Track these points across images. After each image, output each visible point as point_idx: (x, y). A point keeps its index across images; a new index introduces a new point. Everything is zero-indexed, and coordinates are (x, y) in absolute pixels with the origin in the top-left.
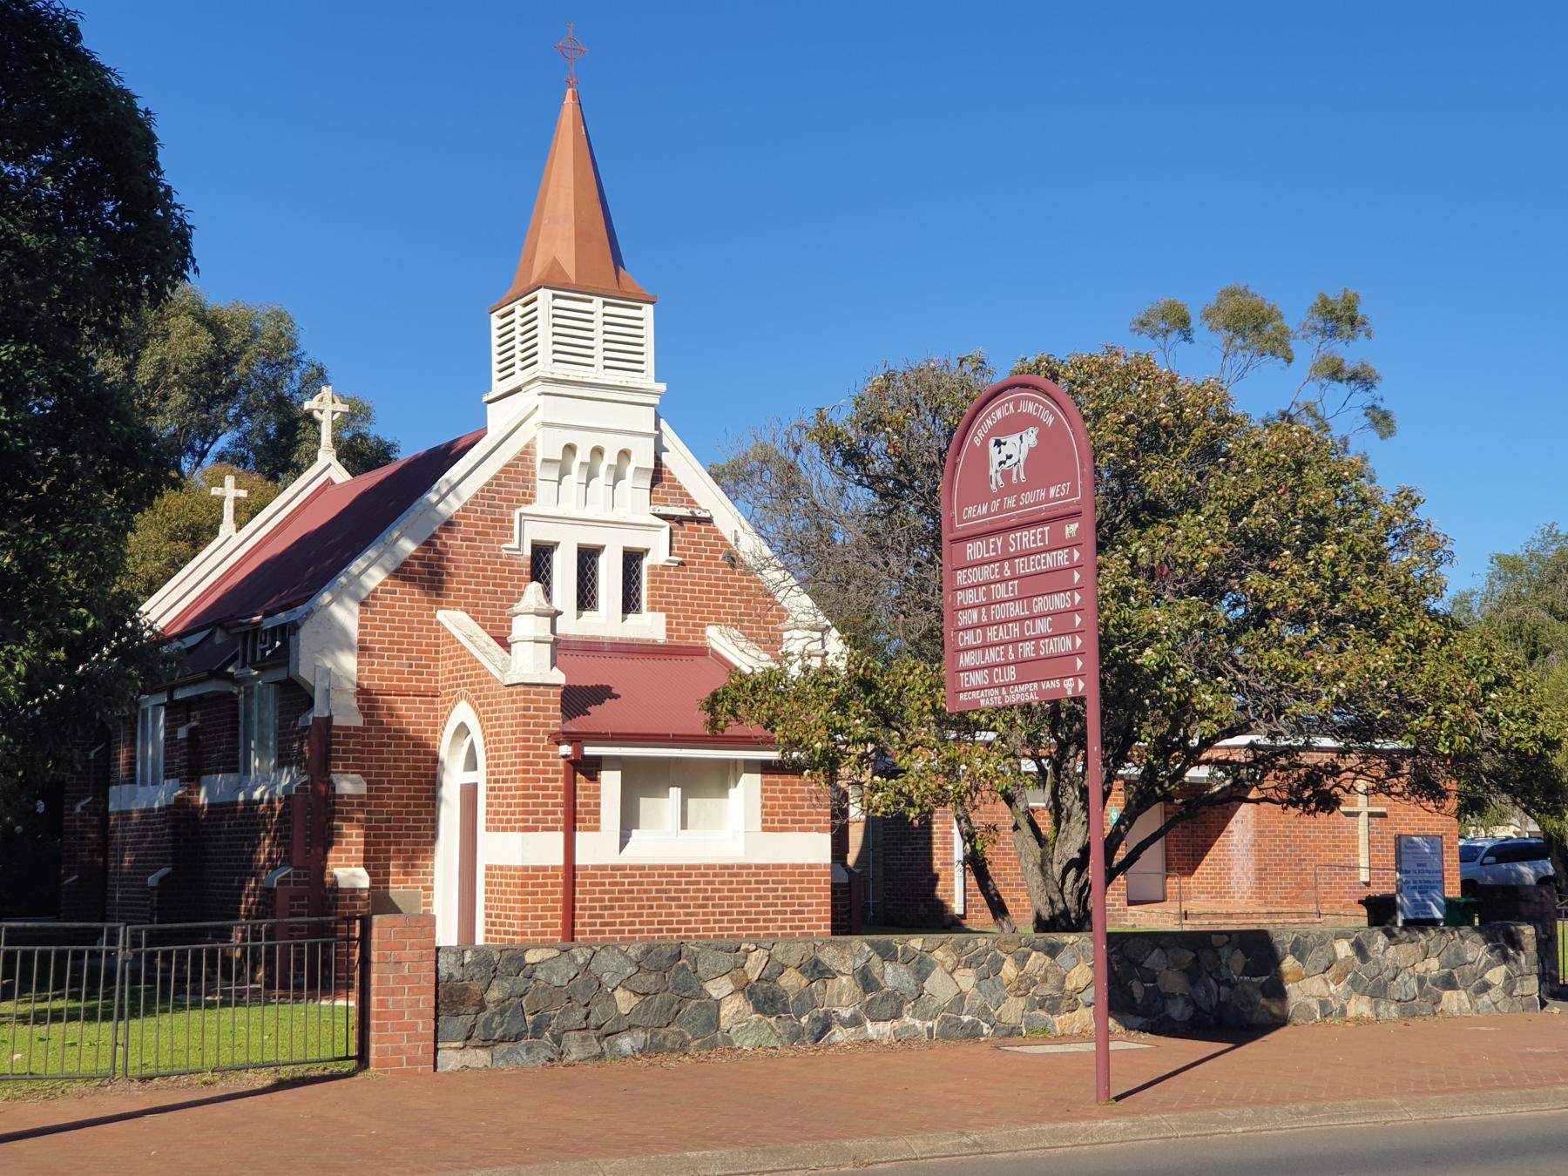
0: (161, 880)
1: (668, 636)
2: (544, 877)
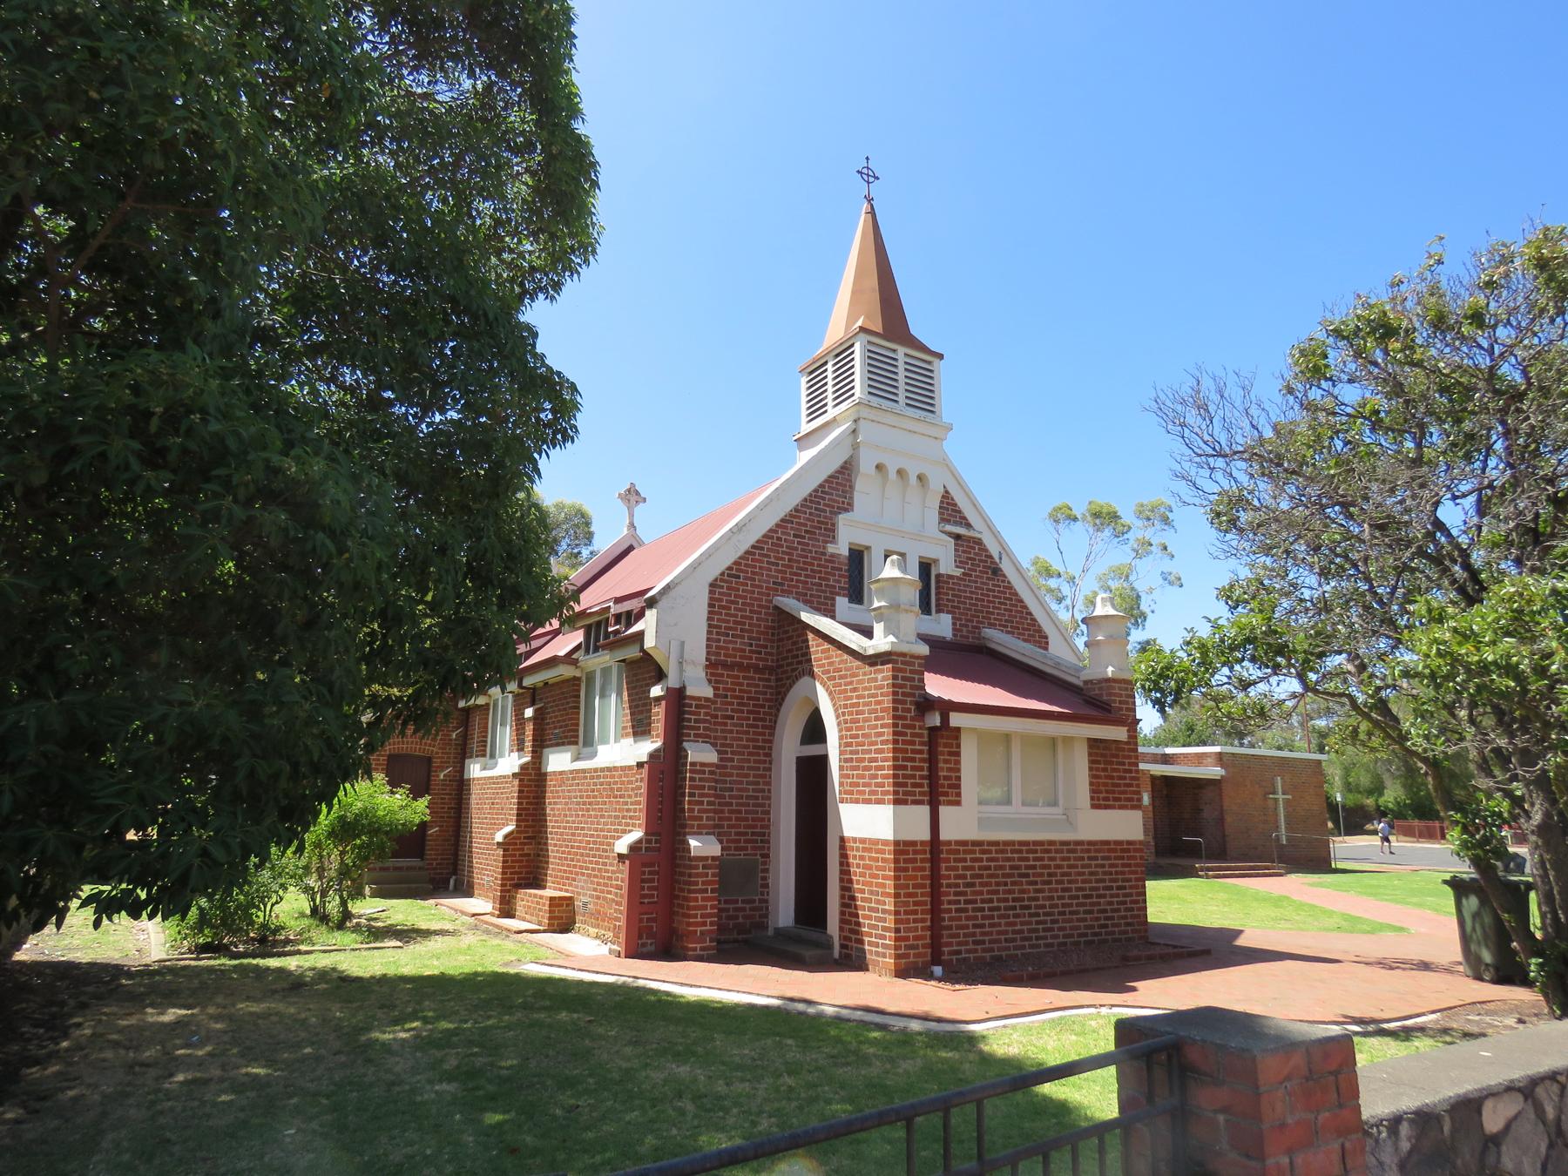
0: (506, 837)
1: (954, 635)
2: (915, 852)
